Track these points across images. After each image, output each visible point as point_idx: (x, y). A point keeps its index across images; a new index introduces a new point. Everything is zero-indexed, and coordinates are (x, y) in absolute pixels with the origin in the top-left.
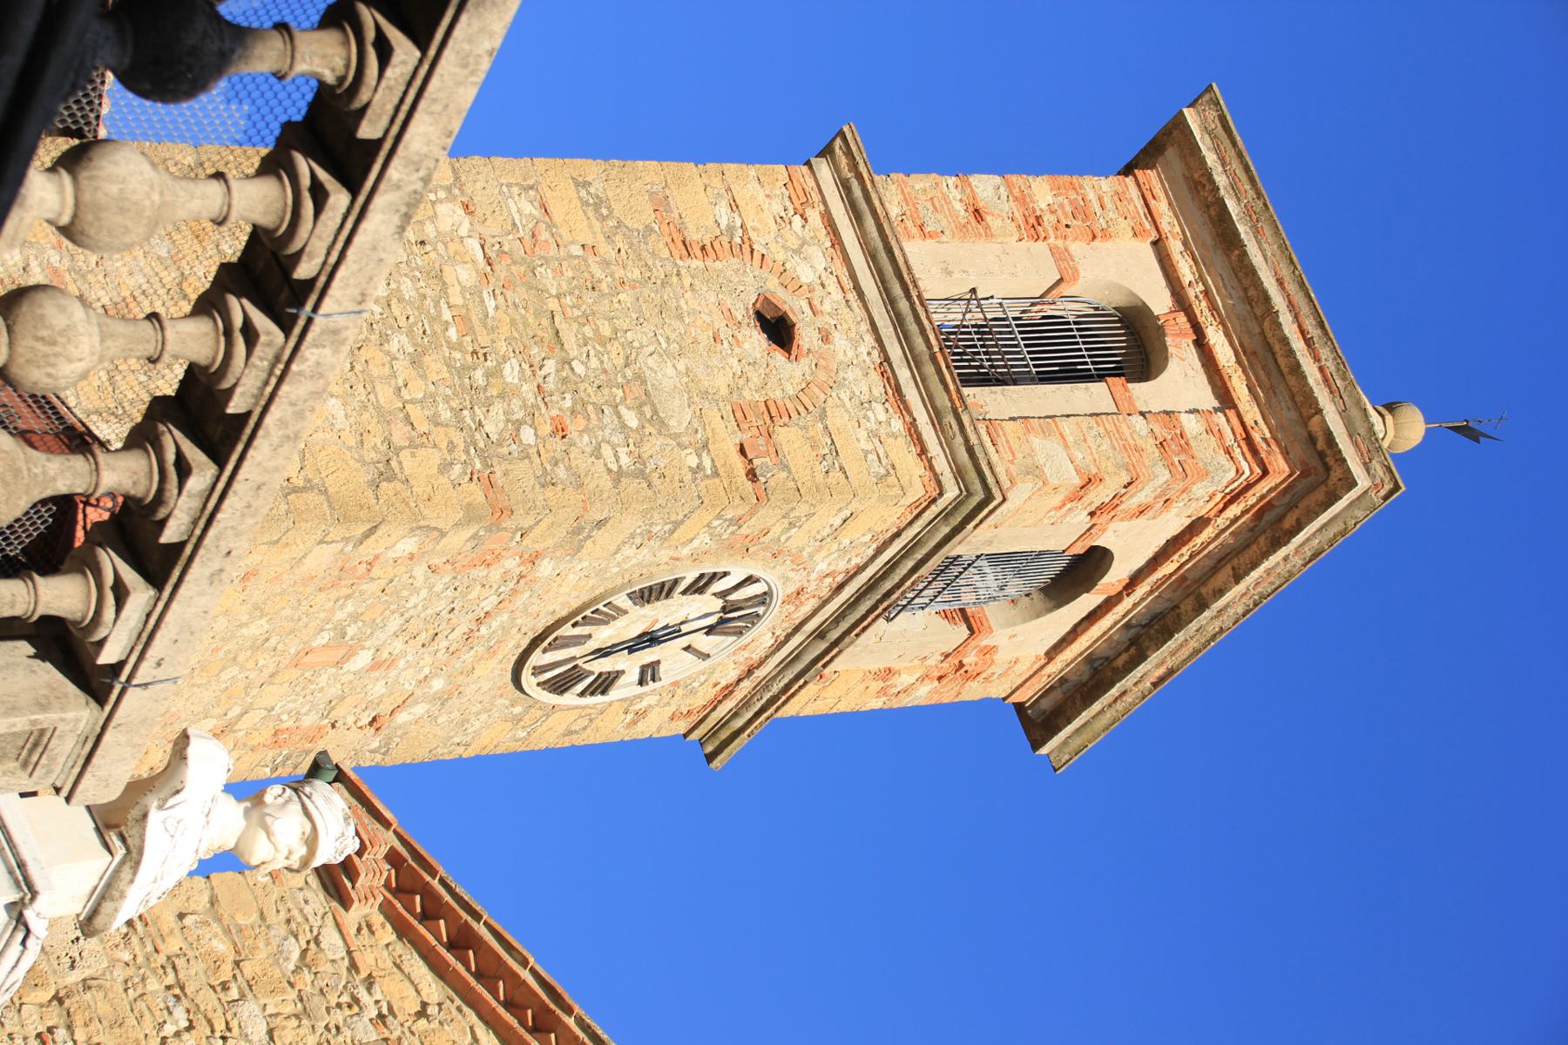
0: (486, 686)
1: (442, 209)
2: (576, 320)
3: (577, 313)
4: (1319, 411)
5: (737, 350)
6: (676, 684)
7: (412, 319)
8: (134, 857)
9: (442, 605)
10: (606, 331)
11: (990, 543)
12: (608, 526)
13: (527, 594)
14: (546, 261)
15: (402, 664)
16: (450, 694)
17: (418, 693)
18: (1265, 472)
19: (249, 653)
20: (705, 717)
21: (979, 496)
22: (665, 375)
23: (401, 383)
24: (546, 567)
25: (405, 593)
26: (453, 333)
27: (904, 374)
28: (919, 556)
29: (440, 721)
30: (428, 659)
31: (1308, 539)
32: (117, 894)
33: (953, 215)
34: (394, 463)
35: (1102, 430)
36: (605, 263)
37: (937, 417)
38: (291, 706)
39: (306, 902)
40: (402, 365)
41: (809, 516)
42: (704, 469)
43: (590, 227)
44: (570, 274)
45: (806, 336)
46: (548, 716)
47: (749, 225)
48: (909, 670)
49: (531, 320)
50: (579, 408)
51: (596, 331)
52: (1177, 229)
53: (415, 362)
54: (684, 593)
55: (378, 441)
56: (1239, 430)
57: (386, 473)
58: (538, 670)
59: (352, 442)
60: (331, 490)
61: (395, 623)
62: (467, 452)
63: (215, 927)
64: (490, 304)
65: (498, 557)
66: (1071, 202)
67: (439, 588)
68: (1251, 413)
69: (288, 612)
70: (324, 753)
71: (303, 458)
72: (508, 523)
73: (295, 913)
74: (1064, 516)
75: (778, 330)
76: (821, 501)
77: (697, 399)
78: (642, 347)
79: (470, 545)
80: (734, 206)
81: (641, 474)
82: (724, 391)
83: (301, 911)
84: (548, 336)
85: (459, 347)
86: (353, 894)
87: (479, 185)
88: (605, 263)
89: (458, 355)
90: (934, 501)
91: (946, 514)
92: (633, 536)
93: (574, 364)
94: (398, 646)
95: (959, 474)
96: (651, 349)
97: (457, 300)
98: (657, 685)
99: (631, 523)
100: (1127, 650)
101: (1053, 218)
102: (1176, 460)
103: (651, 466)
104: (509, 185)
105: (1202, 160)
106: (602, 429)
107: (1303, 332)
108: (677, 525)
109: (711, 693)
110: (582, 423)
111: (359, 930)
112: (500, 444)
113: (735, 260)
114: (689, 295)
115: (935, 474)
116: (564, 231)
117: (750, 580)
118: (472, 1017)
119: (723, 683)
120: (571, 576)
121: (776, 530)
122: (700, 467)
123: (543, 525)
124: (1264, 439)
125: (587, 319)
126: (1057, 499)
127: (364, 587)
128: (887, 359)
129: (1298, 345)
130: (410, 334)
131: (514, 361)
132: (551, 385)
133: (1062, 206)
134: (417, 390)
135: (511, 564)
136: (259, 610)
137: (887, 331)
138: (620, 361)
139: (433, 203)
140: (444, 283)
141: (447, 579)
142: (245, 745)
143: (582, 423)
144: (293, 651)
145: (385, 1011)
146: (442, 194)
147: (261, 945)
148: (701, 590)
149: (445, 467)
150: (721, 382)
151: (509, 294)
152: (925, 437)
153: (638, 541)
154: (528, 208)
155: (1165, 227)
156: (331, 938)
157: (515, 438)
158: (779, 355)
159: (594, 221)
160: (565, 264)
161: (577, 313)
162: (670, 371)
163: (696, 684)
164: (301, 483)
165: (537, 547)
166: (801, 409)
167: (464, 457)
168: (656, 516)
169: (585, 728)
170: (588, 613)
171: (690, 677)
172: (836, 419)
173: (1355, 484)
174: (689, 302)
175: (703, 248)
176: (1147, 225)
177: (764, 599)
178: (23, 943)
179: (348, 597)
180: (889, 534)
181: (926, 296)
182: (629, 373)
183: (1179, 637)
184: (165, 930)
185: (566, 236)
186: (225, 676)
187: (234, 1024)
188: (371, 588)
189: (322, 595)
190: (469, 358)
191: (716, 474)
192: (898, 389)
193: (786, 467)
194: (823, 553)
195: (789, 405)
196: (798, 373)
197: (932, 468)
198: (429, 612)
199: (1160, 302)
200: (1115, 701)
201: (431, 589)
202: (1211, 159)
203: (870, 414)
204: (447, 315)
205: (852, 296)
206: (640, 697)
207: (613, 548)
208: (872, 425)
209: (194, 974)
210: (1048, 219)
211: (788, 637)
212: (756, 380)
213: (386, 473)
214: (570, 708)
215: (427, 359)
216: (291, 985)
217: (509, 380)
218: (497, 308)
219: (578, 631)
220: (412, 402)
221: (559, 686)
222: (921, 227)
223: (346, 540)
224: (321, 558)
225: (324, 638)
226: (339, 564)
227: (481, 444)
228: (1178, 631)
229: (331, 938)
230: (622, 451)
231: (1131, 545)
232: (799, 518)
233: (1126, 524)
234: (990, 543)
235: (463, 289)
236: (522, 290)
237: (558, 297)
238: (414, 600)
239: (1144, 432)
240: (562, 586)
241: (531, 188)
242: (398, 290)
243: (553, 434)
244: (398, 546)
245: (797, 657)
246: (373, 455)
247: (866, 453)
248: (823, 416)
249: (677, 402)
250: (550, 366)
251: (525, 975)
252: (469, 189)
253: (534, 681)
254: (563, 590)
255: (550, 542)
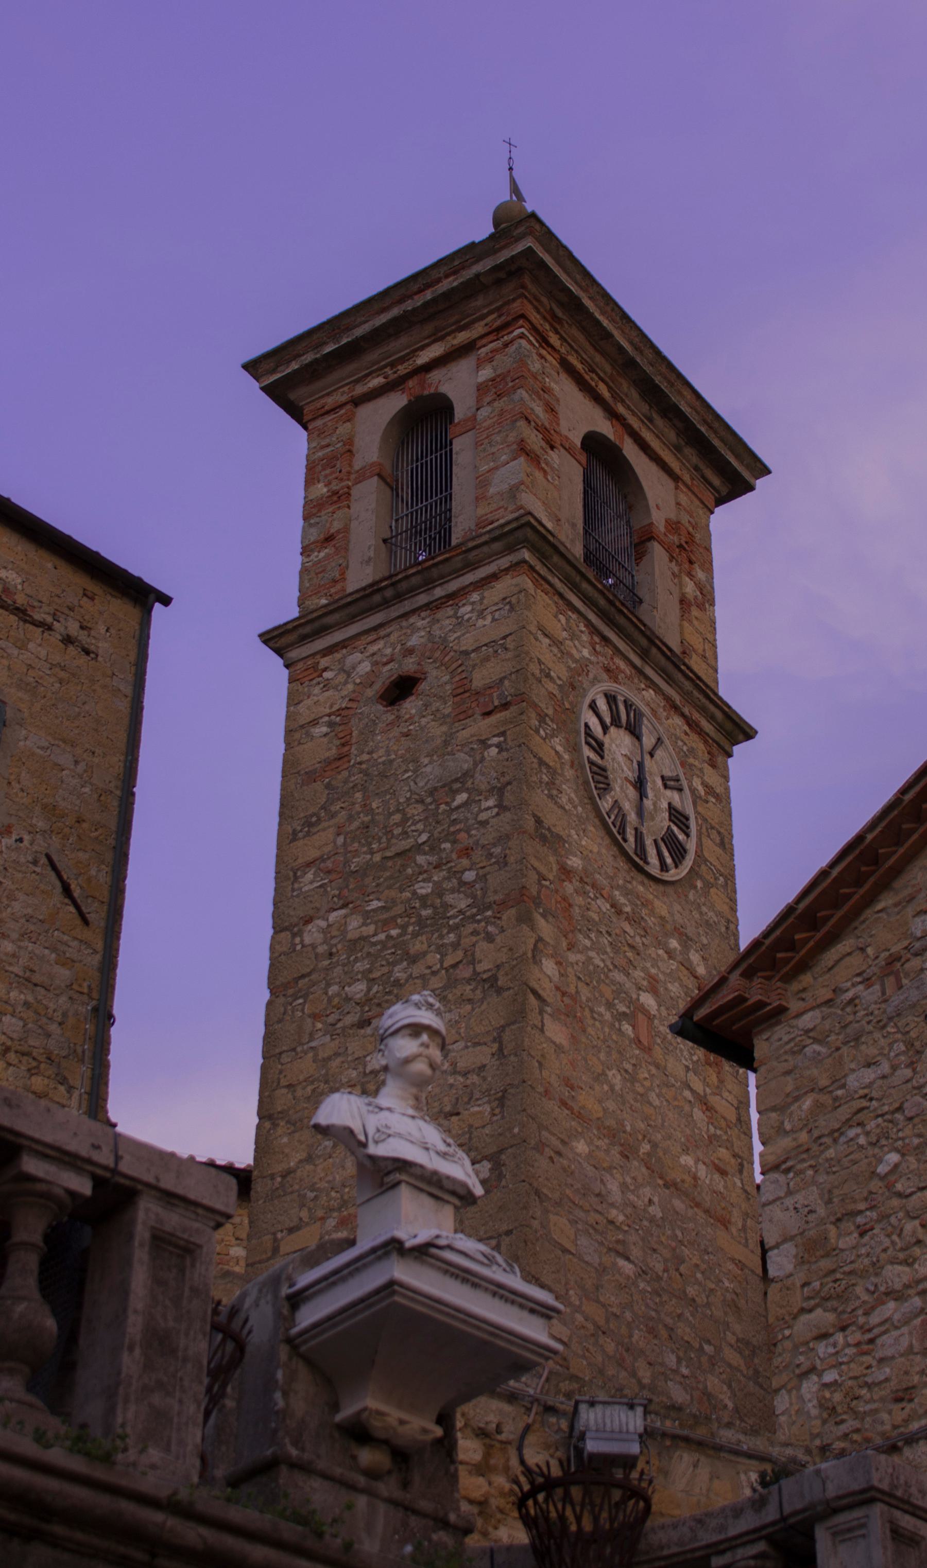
0: (677, 907)
1: (307, 940)
2: (389, 840)
3: (384, 840)
4: (478, 276)
5: (416, 719)
6: (683, 764)
7: (384, 963)
8: (403, 1165)
9: (605, 940)
10: (397, 817)
11: (574, 525)
12: (540, 815)
13: (597, 876)
14: (347, 863)
15: (653, 971)
16: (681, 934)
17: (679, 958)
18: (523, 316)
19: (637, 1085)
20: (714, 741)
21: (529, 532)
22: (431, 771)
23: (428, 971)
24: (575, 862)
25: (591, 968)
26: (394, 932)
27: (439, 592)
28: (578, 579)
29: (705, 941)
30: (652, 951)
31: (576, 283)
32: (435, 1178)
33: (327, 557)
34: (485, 976)
35: (486, 441)
36: (351, 818)
37: (471, 566)
38: (685, 1053)
39: (780, 1039)
40: (417, 970)
41: (540, 662)
42: (500, 743)
43: (324, 830)
44: (356, 845)
45: (409, 666)
46: (706, 860)
47: (328, 711)
48: (681, 585)
49: (388, 874)
50: (451, 838)
51: (397, 825)
52: (346, 389)
53: (414, 960)
54: (602, 757)
55: (469, 988)
56: (491, 337)
57: (491, 983)
58: (664, 867)
59: (469, 1007)
60: (502, 1022)
61: (618, 976)
62: (479, 922)
63: (794, 1107)
64: (375, 904)
65: (565, 899)
66: (324, 469)
67: (587, 943)
68: (479, 329)
69: (602, 1056)
70: (671, 1027)
71: (479, 1044)
72: (534, 891)
73: (788, 1047)
74: (552, 468)
75: (401, 689)
76: (527, 653)
77: (450, 749)
78: (410, 790)
79: (551, 919)
80: (315, 722)
81: (501, 791)
82: (444, 728)
83: (787, 1043)
84: (399, 862)
85: (404, 927)
86: (775, 1004)
87: (292, 913)
88: (351, 818)
89: (411, 928)
90: (532, 568)
91: (543, 558)
92: (550, 796)
93: (420, 841)
94: (638, 974)
95: (510, 549)
96: (412, 783)
97: (372, 928)
98: (682, 777)
99: (539, 798)
100: (670, 420)
101: (334, 483)
102: (511, 384)
103: (495, 783)
104: (293, 890)
105: (295, 372)
106: (467, 819)
107: (420, 291)
108: (541, 762)
109: (694, 736)
110: (463, 835)
111: (803, 999)
112: (474, 897)
113: (352, 722)
114: (375, 756)
115: (511, 567)
116: (326, 850)
117: (593, 706)
118: (868, 913)
119: (686, 728)
120: (584, 843)
121: (551, 687)
122: (498, 746)
123: (536, 864)
124: (500, 316)
125: (389, 832)
126: (539, 475)
127: (584, 999)
128: (427, 606)
129: (428, 295)
130: (394, 964)
131: (416, 886)
132: (433, 859)
133: (326, 476)
134: (433, 958)
135: (569, 888)
136: (600, 1077)
137: (407, 606)
138: (420, 808)
139: (303, 946)
140: (360, 938)
141: (580, 937)
142: (718, 1087)
143: (463, 835)
144: (637, 1052)
145: (859, 979)
146: (297, 940)
147: (808, 1073)
148: (601, 745)
149: (490, 938)
150: (438, 731)
151: (369, 890)
152: (483, 575)
153: (555, 792)
154: (310, 876)
155: (344, 399)
156: (807, 1021)
157: (471, 885)
158: (423, 686)
159: (320, 827)
160: (350, 849)
161: (384, 840)
162: (428, 769)
163: (685, 748)
164: (496, 1045)
165: (555, 867)
166: (460, 670)
167: (483, 924)
168: (534, 779)
169: (719, 833)
170: (615, 831)
171: (678, 754)
172: (468, 643)
173: (530, 248)
174: (380, 755)
175: (343, 745)
176: (343, 412)
177: (611, 699)
178: (440, 1248)
179: (592, 1011)
180: (561, 602)
181: (387, 574)
182: (429, 800)
183: (657, 380)
184: (794, 1144)
185: (330, 848)
186: (657, 1102)
187: (862, 1092)
188: (585, 993)
189: (589, 1030)
190: (413, 920)
191: (503, 734)
192: (451, 596)
193: (501, 680)
194: (574, 652)
195: (457, 679)
196: (434, 673)
197: (507, 570)
198: (608, 950)
199: (396, 402)
200: (711, 428)
201: (587, 948)
202: (295, 366)
203: (466, 617)
204: (382, 936)
205: (382, 633)
206: (693, 791)
207: (560, 811)
208: (474, 616)
209: (826, 1123)
210: (334, 487)
211: (647, 678)
212: (437, 704)
213: (491, 983)
214: (700, 844)
215: (412, 952)
216: (838, 1049)
217: (429, 890)
218: (379, 899)
219: (631, 839)
220: (442, 962)
221: (679, 853)
222: (335, 581)
223: (541, 1012)
224: (556, 1032)
225: (627, 1028)
226: (563, 1017)
227: (475, 910)
228: (653, 380)
229: (807, 1021)
230: (485, 804)
231: (580, 417)
232: (541, 670)
233: (563, 423)
234: (574, 525)
235: (364, 924)
236: (367, 880)
237: (372, 853)
238: (597, 961)
239: (489, 409)
240: (588, 847)
241: (295, 874)
242: (363, 973)
243: (468, 856)
244: (549, 973)
245: (664, 671)
246: (478, 992)
247: (494, 620)
248: (466, 653)
249: (451, 764)
250: (421, 859)
251: (835, 872)
252: (295, 920)
253: (673, 871)
254: (595, 850)
255: (552, 859)
